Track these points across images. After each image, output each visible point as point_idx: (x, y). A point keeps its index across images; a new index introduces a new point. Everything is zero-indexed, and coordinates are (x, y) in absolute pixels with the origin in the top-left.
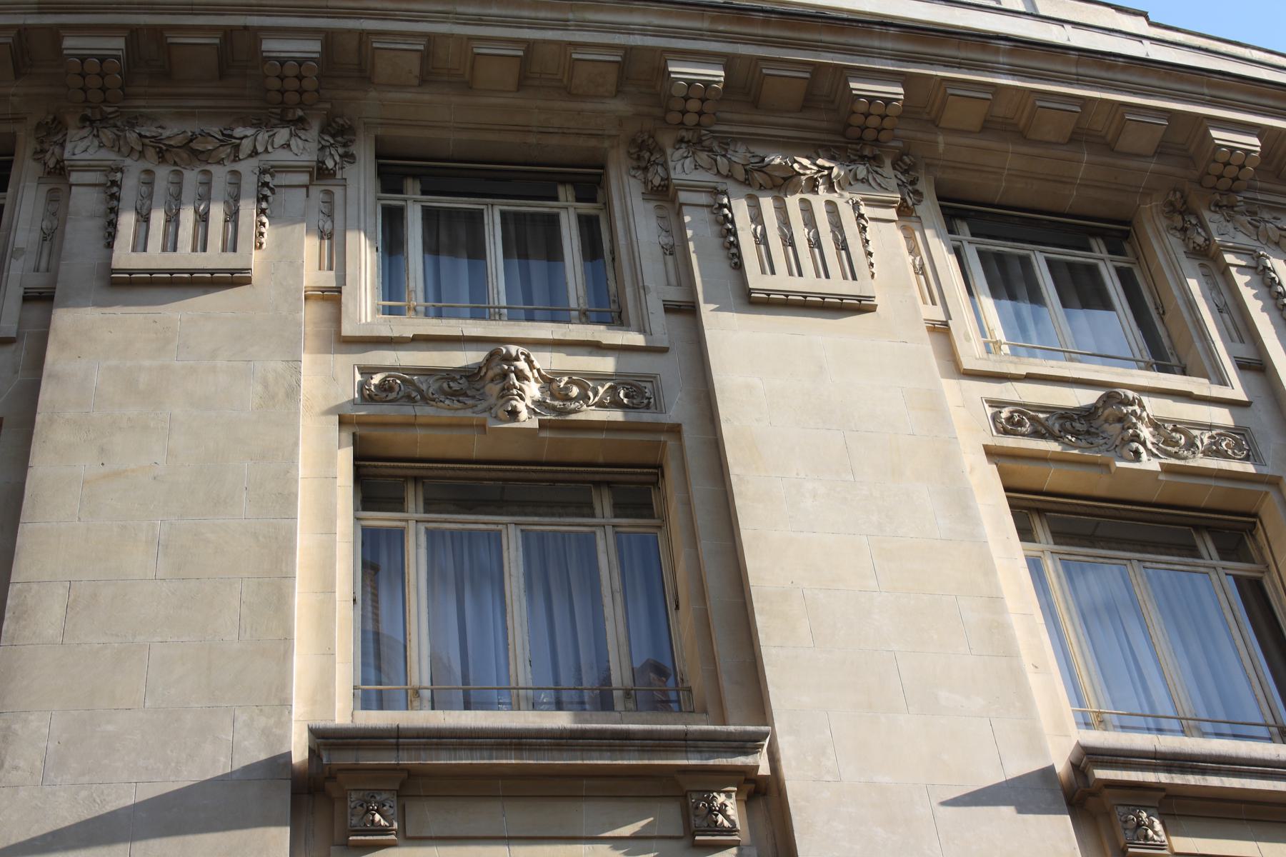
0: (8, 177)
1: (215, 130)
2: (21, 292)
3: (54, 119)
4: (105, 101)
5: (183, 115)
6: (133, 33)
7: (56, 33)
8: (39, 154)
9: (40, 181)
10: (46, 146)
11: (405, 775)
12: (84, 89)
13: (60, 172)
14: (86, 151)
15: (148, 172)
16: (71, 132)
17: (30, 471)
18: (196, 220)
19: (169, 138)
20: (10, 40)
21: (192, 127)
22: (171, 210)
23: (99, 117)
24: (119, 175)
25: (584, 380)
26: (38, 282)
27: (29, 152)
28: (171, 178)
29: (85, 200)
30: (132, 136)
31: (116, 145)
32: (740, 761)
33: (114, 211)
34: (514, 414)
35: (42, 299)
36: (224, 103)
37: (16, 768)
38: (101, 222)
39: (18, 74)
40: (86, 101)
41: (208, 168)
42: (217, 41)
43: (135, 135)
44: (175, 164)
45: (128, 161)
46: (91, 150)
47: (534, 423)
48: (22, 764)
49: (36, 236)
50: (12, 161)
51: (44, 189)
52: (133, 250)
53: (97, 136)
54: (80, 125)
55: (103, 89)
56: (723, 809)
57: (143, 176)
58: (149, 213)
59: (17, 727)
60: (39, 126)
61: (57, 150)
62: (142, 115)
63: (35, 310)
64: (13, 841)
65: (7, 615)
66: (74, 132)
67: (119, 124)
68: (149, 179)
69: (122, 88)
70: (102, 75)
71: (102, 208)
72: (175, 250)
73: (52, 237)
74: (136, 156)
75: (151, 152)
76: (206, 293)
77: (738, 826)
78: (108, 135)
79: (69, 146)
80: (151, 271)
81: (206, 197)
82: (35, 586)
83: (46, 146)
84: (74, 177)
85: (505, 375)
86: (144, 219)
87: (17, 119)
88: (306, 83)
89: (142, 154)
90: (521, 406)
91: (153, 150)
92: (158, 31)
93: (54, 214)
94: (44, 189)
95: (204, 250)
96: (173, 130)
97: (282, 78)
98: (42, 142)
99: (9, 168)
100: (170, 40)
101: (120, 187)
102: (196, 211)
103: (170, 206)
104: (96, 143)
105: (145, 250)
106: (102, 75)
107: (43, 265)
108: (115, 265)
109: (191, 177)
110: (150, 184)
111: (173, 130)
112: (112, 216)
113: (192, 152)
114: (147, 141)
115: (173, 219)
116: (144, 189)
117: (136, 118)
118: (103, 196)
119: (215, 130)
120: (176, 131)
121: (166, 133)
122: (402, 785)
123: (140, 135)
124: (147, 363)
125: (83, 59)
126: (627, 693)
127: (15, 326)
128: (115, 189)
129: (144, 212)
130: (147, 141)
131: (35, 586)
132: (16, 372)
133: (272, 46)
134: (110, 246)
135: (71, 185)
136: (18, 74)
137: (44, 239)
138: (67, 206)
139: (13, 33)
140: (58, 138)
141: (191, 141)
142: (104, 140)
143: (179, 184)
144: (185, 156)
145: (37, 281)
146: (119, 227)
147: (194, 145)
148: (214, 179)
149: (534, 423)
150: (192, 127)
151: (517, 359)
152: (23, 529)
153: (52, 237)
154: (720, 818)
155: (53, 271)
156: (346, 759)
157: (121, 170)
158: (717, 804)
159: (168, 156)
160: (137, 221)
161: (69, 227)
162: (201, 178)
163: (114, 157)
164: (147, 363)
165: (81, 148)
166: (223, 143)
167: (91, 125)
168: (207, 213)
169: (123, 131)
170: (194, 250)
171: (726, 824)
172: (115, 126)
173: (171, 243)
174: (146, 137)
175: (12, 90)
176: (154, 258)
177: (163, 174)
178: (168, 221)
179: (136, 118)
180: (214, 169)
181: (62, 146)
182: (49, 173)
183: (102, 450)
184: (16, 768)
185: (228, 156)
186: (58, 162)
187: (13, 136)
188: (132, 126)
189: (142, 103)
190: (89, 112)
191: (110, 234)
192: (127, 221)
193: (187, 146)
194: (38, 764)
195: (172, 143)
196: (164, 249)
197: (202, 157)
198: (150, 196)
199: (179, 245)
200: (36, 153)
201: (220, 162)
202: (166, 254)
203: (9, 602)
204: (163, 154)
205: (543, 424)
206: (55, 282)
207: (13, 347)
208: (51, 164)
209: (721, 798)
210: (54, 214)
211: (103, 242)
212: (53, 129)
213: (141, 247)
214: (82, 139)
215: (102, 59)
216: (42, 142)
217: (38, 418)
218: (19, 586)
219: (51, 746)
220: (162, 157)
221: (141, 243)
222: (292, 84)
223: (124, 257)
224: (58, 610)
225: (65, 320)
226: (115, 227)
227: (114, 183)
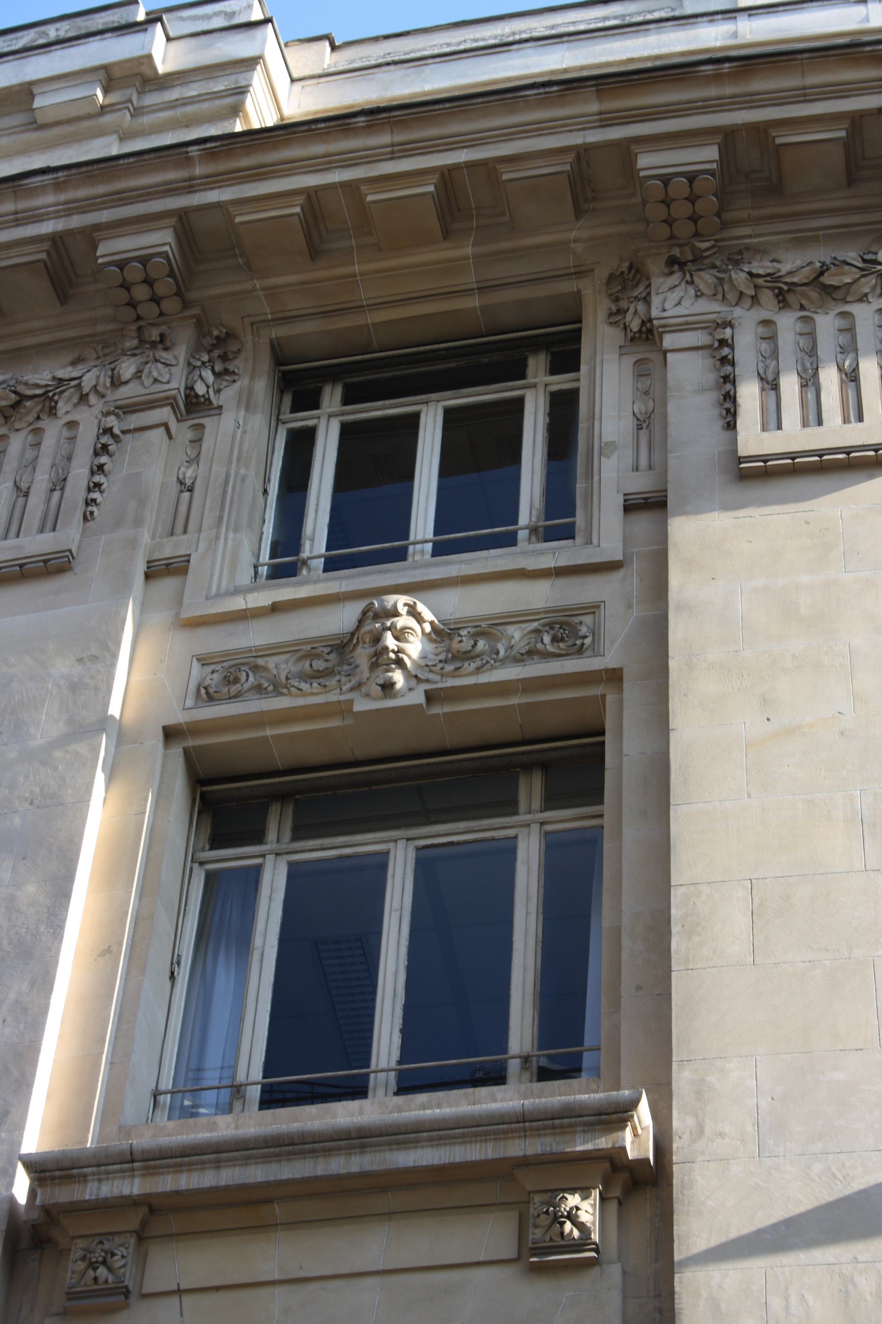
0: (579, 350)
1: (852, 255)
2: (621, 500)
3: (630, 268)
4: (697, 234)
5: (802, 241)
6: (728, 138)
7: (625, 151)
8: (616, 316)
9: (622, 351)
10: (623, 304)
11: (143, 1211)
12: (669, 222)
13: (647, 335)
14: (679, 303)
15: (766, 323)
16: (656, 282)
17: (673, 736)
18: (842, 382)
19: (790, 273)
20: (568, 167)
21: (819, 255)
22: (805, 370)
23: (690, 257)
24: (728, 331)
25: (488, 628)
26: (641, 484)
27: (601, 316)
28: (799, 327)
29: (688, 371)
30: (739, 277)
31: (719, 292)
32: (603, 1142)
33: (729, 380)
34: (388, 687)
35: (650, 506)
36: (856, 218)
37: (721, 1135)
38: (713, 397)
39: (579, 212)
40: (672, 237)
41: (848, 308)
42: (843, 134)
43: (743, 275)
44: (802, 307)
45: (738, 312)
46: (686, 303)
47: (417, 698)
48: (728, 1129)
49: (629, 424)
50: (579, 330)
51: (629, 360)
52: (764, 429)
53: (692, 283)
54: (666, 270)
55: (694, 219)
56: (572, 1216)
57: (761, 330)
58: (777, 374)
59: (712, 1079)
60: (611, 278)
61: (641, 307)
62: (747, 248)
63: (643, 522)
64: (734, 1234)
65: (674, 930)
66: (662, 279)
67: (718, 263)
68: (769, 332)
69: (718, 215)
70: (692, 199)
71: (711, 378)
72: (820, 423)
73: (650, 424)
74: (747, 302)
75: (767, 297)
76: (871, 477)
77: (595, 1237)
78: (706, 279)
79: (656, 301)
80: (793, 456)
81: (850, 347)
82: (705, 889)
83: (623, 304)
84: (669, 341)
85: (377, 639)
86: (771, 385)
87: (580, 273)
88: (700, 207)
89: (755, 300)
90: (398, 677)
91: (769, 293)
92: (761, 130)
93: (646, 393)
94: (629, 360)
95: (860, 419)
96: (793, 263)
97: (667, 202)
98: (617, 300)
99: (578, 340)
100: (779, 141)
101: (732, 347)
102: (840, 369)
103: (803, 366)
104: (691, 291)
105: (779, 427)
106: (692, 199)
107: (643, 461)
108: (743, 451)
109: (826, 323)
110: (772, 338)
111: (793, 263)
112: (728, 386)
113: (824, 289)
114: (760, 281)
115: (810, 381)
116: (764, 346)
117: (740, 252)
118: (709, 362)
119: (852, 255)
120: (799, 263)
121: (785, 268)
122: (144, 1224)
123: (750, 274)
124: (805, 579)
125: (666, 180)
126: (526, 1060)
127: (620, 546)
128: (726, 351)
129: (770, 377)
130: (760, 281)
131: (705, 889)
132: (630, 606)
133: (648, 161)
134: (731, 426)
135: (665, 353)
136: (579, 212)
137: (639, 428)
138: (664, 380)
139: (571, 157)
140: (640, 290)
141: (822, 273)
142: (702, 286)
143: (811, 335)
144: (814, 295)
145: (640, 484)
146: (740, 400)
147: (827, 280)
148: (858, 322)
149: (417, 698)
150: (819, 255)
151: (395, 614)
152: (675, 813)
153: (650, 424)
154: (568, 1226)
155: (658, 466)
156: (65, 1195)
157: (730, 324)
158: (565, 1207)
159: (791, 298)
160: (763, 389)
161: (671, 408)
162: (839, 323)
163: (718, 309)
164: (805, 579)
165: (673, 301)
166: (865, 273)
167: (681, 269)
168: (856, 369)
169: (726, 271)
170: (846, 420)
171: (576, 1233)
172: (714, 267)
173: (814, 415)
174: (759, 276)
175: (573, 234)
176: (793, 437)
177: (787, 323)
178: (804, 386)
179: (740, 252)
180: (855, 309)
181: (647, 300)
182: (632, 339)
183: (764, 701)
184: (721, 1135)
185: (873, 289)
186: (643, 323)
187: (578, 296)
188: (737, 263)
189: (746, 231)
190: (676, 252)
191: (728, 411)
192: (749, 394)
193: (816, 281)
194: (750, 1128)
195: (795, 279)
196: (805, 424)
197: (838, 295)
198: (775, 354)
199: (825, 416)
200: (611, 315)
201: (863, 299)
202: (809, 430)
203: (673, 911)
204: (784, 294)
205: (430, 697)
206: (666, 482)
207: (620, 574)
208: (635, 326)
209: (573, 1200)
210: (646, 393)
211: (721, 423)
212: (629, 280)
213: (773, 423)
214: (672, 288)
215: (691, 177)
216: (617, 300)
217: (673, 664)
218: (683, 889)
219: (764, 1103)
220: (783, 300)
221: (773, 419)
222: (681, 210)
223: (753, 439)
224: (742, 921)
225: (685, 531)
226: (734, 400)
227: (723, 343)
